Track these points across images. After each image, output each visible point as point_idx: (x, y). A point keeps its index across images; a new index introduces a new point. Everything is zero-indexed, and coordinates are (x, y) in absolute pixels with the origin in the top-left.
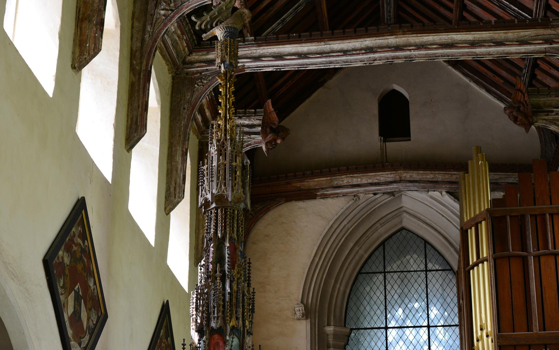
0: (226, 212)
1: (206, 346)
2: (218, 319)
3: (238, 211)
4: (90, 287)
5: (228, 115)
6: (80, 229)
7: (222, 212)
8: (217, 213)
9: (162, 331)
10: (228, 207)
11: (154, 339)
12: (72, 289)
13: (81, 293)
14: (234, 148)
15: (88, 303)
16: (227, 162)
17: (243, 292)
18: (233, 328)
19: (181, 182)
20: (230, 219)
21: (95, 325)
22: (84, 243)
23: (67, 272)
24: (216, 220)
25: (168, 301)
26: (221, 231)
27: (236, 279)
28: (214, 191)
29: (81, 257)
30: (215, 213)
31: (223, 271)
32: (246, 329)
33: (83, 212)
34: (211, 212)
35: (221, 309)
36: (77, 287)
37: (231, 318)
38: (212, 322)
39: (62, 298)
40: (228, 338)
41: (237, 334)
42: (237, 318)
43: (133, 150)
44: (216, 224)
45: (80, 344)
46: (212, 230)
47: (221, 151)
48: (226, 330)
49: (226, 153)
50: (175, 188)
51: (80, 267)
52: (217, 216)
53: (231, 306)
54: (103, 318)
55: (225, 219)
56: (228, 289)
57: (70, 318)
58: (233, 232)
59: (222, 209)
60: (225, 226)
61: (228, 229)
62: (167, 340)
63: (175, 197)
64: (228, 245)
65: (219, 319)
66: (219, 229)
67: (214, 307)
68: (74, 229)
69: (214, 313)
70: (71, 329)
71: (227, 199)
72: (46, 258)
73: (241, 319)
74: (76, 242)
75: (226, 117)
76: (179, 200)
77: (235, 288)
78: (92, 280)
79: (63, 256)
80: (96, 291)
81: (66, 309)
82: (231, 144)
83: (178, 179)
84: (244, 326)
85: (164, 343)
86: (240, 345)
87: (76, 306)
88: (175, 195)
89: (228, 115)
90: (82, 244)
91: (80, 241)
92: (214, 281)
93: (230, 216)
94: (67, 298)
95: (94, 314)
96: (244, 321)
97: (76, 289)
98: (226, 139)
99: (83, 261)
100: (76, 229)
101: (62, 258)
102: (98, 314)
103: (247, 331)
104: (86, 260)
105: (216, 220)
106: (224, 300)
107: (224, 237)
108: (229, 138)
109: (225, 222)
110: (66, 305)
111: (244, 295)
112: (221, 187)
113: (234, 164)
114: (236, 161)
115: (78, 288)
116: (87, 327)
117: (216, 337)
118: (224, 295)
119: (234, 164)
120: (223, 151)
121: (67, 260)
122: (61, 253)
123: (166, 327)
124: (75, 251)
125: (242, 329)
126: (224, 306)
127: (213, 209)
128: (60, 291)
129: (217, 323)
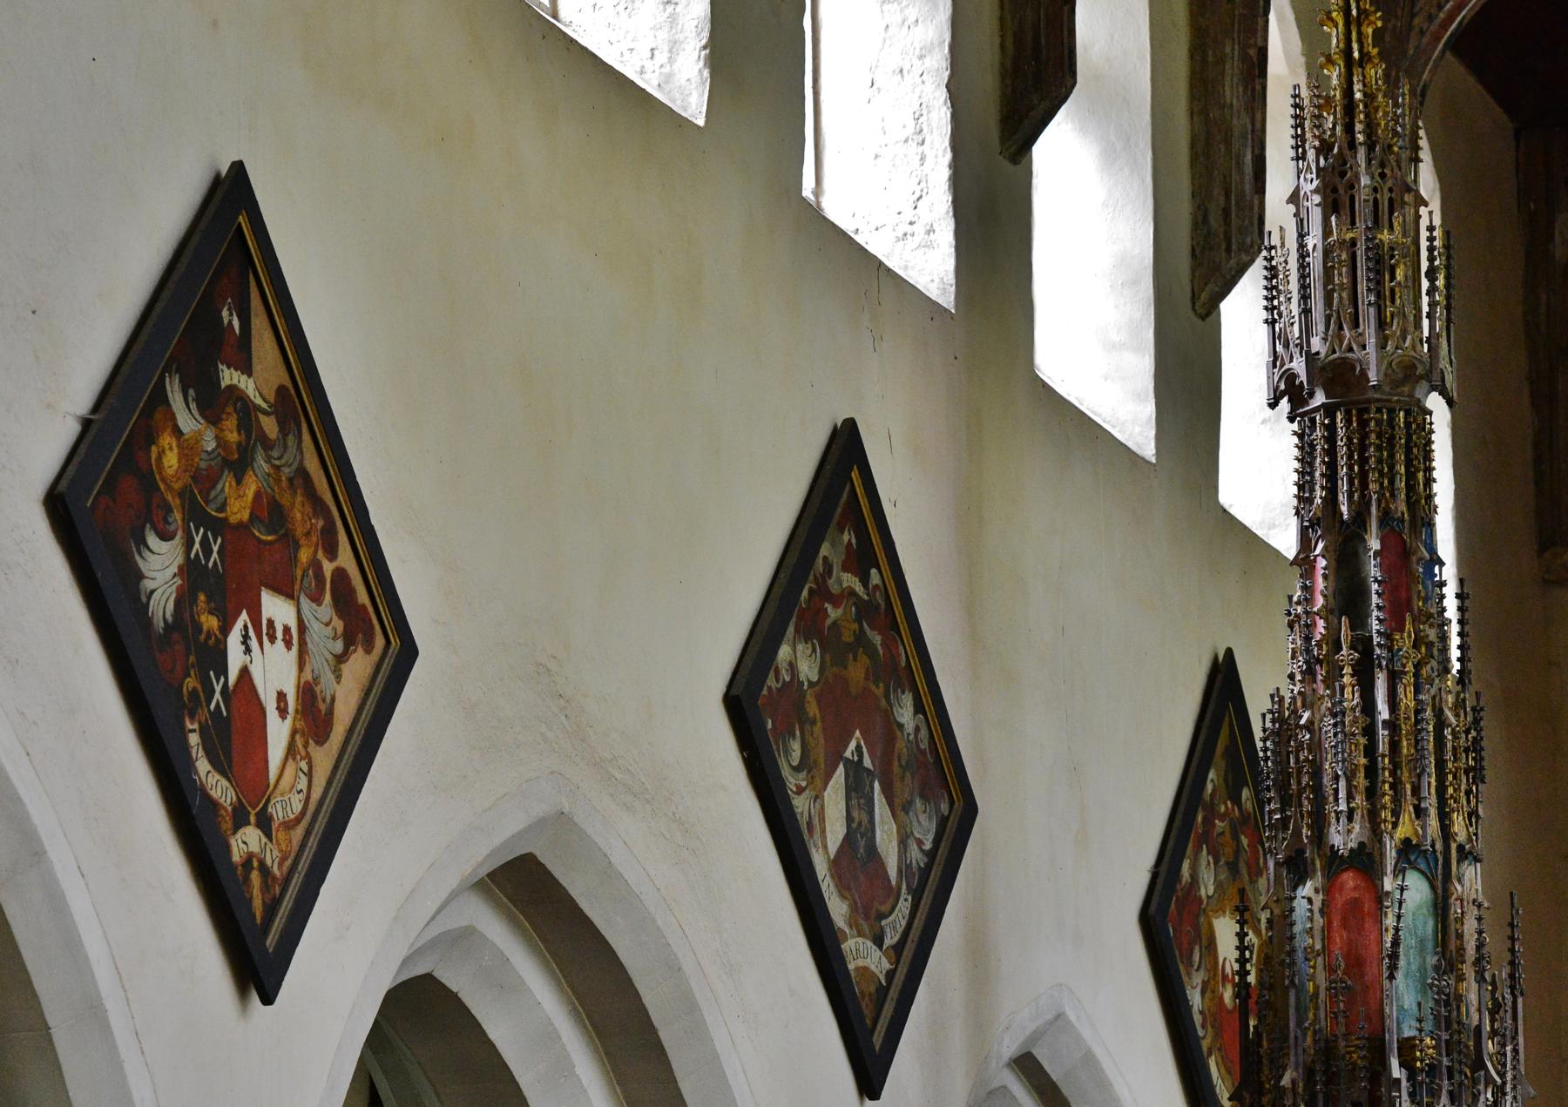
0: (1363, 424)
1: (1317, 916)
2: (1350, 819)
3: (1408, 413)
4: (901, 726)
5: (1355, 46)
6: (846, 537)
7: (1348, 422)
8: (1331, 429)
9: (1211, 775)
10: (1369, 401)
11: (1179, 817)
12: (836, 756)
13: (867, 762)
14: (1383, 175)
15: (897, 785)
16: (1359, 232)
17: (1438, 714)
18: (1407, 849)
19: (1248, 187)
20: (1379, 448)
21: (931, 855)
22: (865, 581)
23: (813, 709)
24: (1331, 452)
25: (1229, 652)
26: (1350, 497)
27: (1410, 667)
28: (1316, 344)
29: (860, 637)
30: (1326, 427)
31: (1363, 645)
32: (1454, 846)
33: (855, 475)
34: (1313, 421)
35: (1361, 781)
36: (852, 745)
37: (1396, 813)
38: (1332, 829)
39: (801, 804)
40: (1388, 884)
41: (1423, 866)
42: (1420, 812)
43: (1035, 148)
44: (1332, 466)
45: (878, 941)
46: (1318, 492)
47: (1335, 190)
48: (1382, 855)
49: (1352, 198)
50: (1226, 212)
51: (857, 671)
52: (1331, 439)
53: (1396, 767)
54: (959, 819)
55: (1363, 448)
56: (1383, 712)
57: (835, 864)
58: (1393, 495)
59: (1348, 414)
60: (1364, 475)
61: (1373, 486)
62: (1237, 800)
63: (1228, 250)
64: (1375, 544)
65: (1357, 817)
66: (1343, 486)
67: (1336, 778)
68: (825, 550)
69: (1336, 799)
70: (842, 896)
71: (1364, 374)
72: (734, 692)
73: (1433, 812)
74: (835, 589)
75: (1348, 52)
76: (1245, 258)
77: (1407, 700)
78: (907, 699)
79: (800, 660)
80: (924, 732)
81: (817, 836)
82: (1369, 161)
83: (1235, 177)
84: (1446, 833)
85: (1222, 818)
86: (1435, 905)
87: (855, 814)
88: (1228, 239)
89: (1355, 46)
90: (859, 588)
91: (850, 581)
92: (1334, 674)
93: (1379, 436)
94: (817, 797)
95: (923, 817)
96: (1444, 816)
97: (848, 754)
98: (1352, 145)
99: (871, 652)
100: (833, 545)
101: (792, 667)
102: (938, 809)
103: (1461, 848)
104: (877, 639)
105: (1331, 452)
106: (1371, 750)
107: (1360, 517)
108: (1360, 138)
109: (1363, 461)
110: (816, 821)
111: (1441, 724)
112: (1341, 328)
113: (1385, 236)
114: (1391, 227)
115: (858, 747)
116: (900, 871)
117: (1349, 880)
118: (1370, 731)
119: (1385, 236)
120: (1341, 191)
121: (808, 669)
122: (784, 652)
123: (1231, 754)
124: (835, 623)
125: (1439, 846)
126: (1371, 771)
127: (1317, 409)
128: (792, 780)
129: (1349, 831)
